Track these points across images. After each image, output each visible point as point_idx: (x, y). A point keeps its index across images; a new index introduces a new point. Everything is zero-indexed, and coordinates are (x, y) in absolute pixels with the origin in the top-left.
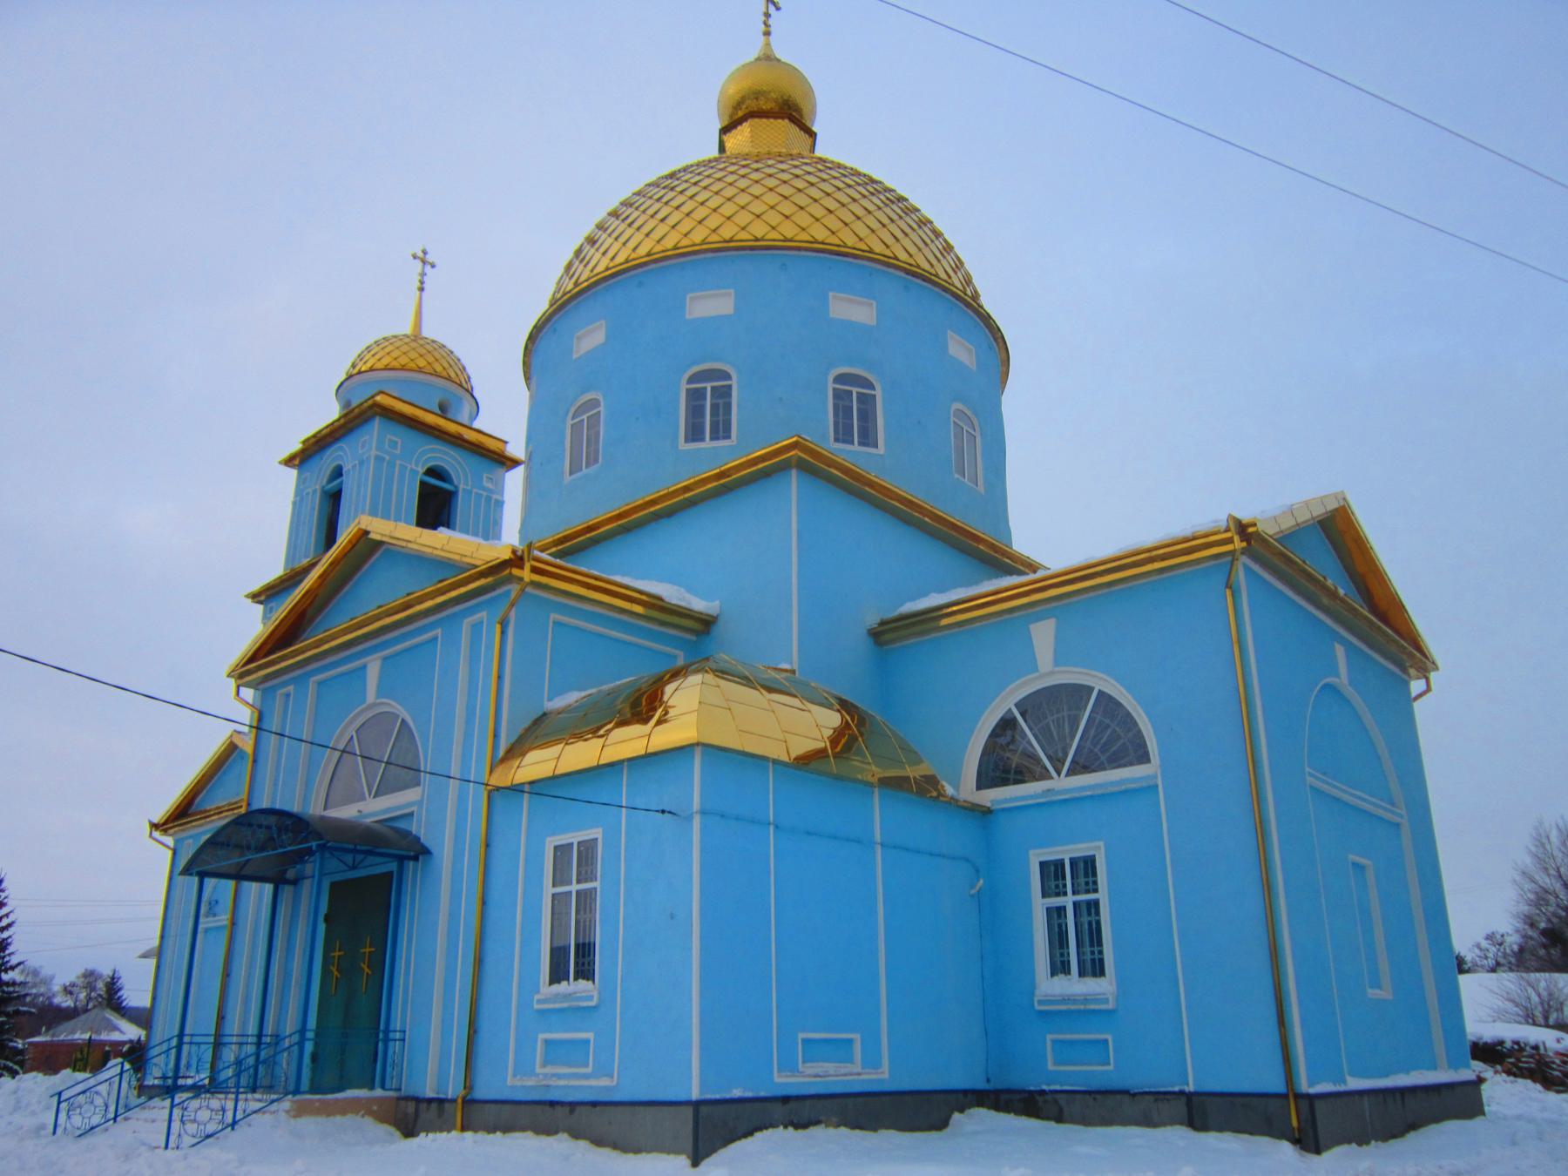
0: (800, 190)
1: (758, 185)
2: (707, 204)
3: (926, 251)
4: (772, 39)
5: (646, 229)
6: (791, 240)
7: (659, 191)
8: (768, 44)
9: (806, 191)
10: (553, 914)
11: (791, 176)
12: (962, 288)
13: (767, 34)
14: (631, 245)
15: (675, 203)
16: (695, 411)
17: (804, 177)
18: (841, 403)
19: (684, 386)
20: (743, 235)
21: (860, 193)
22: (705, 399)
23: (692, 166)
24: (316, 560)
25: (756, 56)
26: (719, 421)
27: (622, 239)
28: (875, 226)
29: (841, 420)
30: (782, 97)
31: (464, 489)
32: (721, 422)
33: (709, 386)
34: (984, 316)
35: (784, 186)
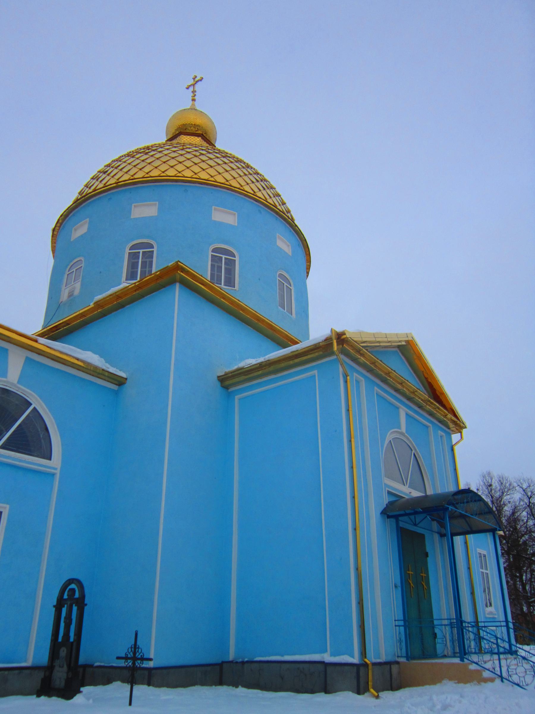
1: (189, 161)
4: (196, 103)
7: (117, 163)
9: (207, 170)
13: (194, 100)
15: (139, 167)
18: (216, 264)
19: (127, 251)
21: (256, 179)
22: (139, 258)
26: (146, 270)
29: (216, 273)
30: (471, 685)
32: (147, 267)
33: (141, 251)
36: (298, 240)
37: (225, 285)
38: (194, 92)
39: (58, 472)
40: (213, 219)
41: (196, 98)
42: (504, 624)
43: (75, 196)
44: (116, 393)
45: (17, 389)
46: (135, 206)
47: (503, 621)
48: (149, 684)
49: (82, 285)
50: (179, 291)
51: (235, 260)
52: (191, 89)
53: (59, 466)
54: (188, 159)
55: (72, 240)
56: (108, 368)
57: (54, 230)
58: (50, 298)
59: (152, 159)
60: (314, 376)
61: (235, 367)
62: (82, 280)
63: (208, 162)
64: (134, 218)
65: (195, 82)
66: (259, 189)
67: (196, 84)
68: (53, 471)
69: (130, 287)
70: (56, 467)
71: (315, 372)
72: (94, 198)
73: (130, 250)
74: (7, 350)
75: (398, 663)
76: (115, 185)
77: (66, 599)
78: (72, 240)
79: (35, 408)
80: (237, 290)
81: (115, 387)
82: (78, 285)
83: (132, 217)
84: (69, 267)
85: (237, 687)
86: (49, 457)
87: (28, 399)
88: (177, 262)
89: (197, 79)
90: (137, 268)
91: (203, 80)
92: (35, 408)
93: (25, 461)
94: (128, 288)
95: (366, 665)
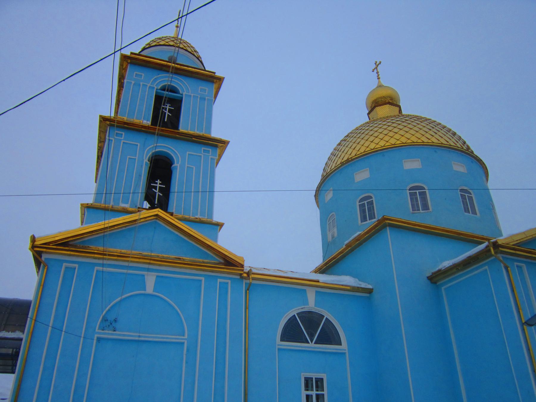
0: (395, 127)
4: (381, 80)
6: (374, 149)
8: (379, 82)
9: (397, 127)
11: (396, 121)
13: (378, 78)
16: (363, 211)
19: (358, 204)
27: (338, 156)
31: (186, 95)
33: (366, 202)
35: (399, 126)
36: (470, 158)
37: (422, 210)
38: (377, 73)
39: (347, 351)
40: (405, 168)
45: (315, 310)
46: (356, 174)
50: (390, 232)
52: (375, 71)
55: (326, 202)
56: (361, 285)
57: (315, 196)
58: (323, 239)
59: (367, 137)
60: (486, 270)
61: (437, 269)
62: (337, 227)
63: (408, 126)
64: (357, 182)
65: (377, 66)
66: (444, 134)
67: (377, 67)
68: (344, 351)
70: (345, 349)
71: (487, 267)
72: (330, 177)
73: (359, 202)
78: (326, 202)
79: (327, 318)
80: (431, 211)
81: (368, 295)
82: (335, 230)
83: (356, 182)
84: (328, 219)
85: (9, 332)
88: (383, 216)
89: (377, 64)
90: (366, 213)
91: (381, 63)
92: (327, 318)
94: (361, 234)
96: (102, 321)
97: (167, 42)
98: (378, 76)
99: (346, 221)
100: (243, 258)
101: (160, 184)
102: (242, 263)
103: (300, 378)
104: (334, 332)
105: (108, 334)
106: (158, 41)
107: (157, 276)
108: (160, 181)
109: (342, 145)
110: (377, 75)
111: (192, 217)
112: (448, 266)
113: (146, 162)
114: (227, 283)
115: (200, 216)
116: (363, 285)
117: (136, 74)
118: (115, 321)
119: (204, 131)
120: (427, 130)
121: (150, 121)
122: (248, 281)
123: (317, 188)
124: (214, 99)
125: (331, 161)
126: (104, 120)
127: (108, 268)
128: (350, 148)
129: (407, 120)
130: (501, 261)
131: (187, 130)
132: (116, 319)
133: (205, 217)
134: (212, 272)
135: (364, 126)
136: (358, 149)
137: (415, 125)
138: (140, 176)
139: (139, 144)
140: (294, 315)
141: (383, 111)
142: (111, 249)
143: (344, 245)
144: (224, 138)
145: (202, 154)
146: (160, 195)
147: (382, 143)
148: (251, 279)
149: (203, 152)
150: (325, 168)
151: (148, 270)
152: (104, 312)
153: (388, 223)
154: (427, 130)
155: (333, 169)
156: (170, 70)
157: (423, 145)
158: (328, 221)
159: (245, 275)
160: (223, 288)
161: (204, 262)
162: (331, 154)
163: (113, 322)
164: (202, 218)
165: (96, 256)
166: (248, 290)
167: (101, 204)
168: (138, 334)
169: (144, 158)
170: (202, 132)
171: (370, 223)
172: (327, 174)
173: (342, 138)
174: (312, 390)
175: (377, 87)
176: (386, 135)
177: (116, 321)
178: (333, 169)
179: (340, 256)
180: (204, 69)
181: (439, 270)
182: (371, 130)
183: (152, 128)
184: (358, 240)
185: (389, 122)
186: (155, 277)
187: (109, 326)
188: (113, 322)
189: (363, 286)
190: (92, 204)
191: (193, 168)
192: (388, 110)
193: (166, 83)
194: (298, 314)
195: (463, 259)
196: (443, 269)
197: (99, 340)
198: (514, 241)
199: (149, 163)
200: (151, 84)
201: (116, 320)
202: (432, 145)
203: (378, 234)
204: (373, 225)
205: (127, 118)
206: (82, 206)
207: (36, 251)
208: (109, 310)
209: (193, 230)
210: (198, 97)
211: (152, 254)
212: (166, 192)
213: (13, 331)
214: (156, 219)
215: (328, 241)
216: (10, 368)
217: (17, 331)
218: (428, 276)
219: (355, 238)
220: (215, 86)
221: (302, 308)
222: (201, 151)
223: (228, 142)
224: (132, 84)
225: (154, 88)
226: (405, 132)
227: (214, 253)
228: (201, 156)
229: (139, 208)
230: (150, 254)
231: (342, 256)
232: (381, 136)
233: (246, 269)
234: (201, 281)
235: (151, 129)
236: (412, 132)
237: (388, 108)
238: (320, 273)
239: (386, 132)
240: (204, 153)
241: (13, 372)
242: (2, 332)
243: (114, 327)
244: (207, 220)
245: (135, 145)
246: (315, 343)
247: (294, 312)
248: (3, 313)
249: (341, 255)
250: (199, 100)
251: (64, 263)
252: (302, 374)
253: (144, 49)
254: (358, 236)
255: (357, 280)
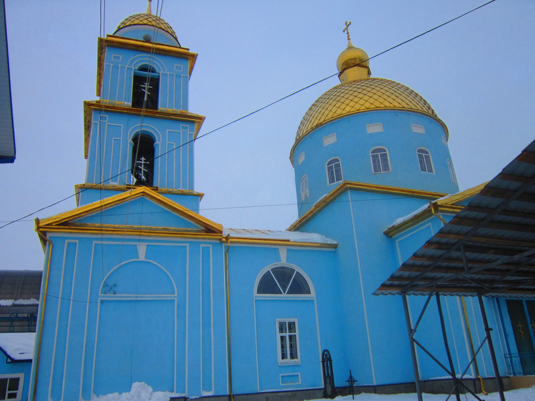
0: (364, 90)
2: (340, 101)
3: (415, 100)
4: (351, 41)
5: (322, 113)
6: (340, 115)
9: (362, 92)
10: (296, 338)
12: (427, 111)
13: (349, 39)
14: (318, 118)
17: (370, 87)
19: (326, 167)
20: (353, 110)
23: (331, 89)
24: (445, 195)
25: (347, 48)
28: (395, 98)
31: (162, 73)
33: (333, 165)
34: (438, 120)
35: (359, 89)
38: (348, 33)
39: (315, 299)
40: (368, 132)
41: (350, 37)
42: (513, 355)
43: (293, 142)
44: (335, 253)
47: (516, 354)
48: (375, 393)
49: (309, 190)
51: (386, 153)
52: (346, 31)
53: (315, 296)
54: (351, 90)
55: (299, 165)
56: (327, 241)
57: (290, 158)
60: (430, 226)
61: (392, 225)
63: (367, 89)
65: (347, 26)
67: (348, 27)
69: (328, 196)
70: (313, 296)
72: (304, 139)
74: (278, 249)
75: (508, 377)
76: (311, 130)
77: (325, 359)
78: (299, 165)
79: (297, 272)
81: (334, 250)
82: (308, 190)
83: (324, 146)
85: (25, 299)
86: (309, 293)
87: (294, 269)
91: (351, 24)
92: (297, 272)
93: (299, 297)
95: (479, 379)
96: (104, 285)
97: (141, 21)
98: (348, 37)
99: (316, 182)
100: (222, 225)
101: (148, 85)
102: (221, 230)
103: (275, 324)
104: (304, 283)
105: (110, 297)
106: (132, 20)
107: (148, 246)
108: (144, 158)
109: (313, 110)
110: (347, 35)
111: (175, 189)
112: (400, 222)
113: (130, 142)
114: (209, 247)
115: (182, 188)
116: (330, 241)
117: (114, 56)
118: (115, 285)
119: (181, 108)
120: (393, 92)
121: (130, 102)
122: (227, 245)
123: (291, 151)
124: (189, 76)
125: (303, 126)
126: (88, 105)
127: (105, 241)
128: (319, 113)
129: (372, 85)
130: (441, 219)
131: (166, 108)
132: (115, 284)
133: (187, 189)
134: (195, 239)
135: (333, 92)
136: (335, 104)
137: (379, 90)
138: (126, 155)
139: (122, 126)
140: (269, 271)
141: (354, 73)
142: (106, 225)
143: (313, 206)
144: (200, 114)
145: (180, 130)
146: (146, 172)
147: (348, 109)
148: (229, 243)
149: (182, 129)
150: (300, 126)
151: (139, 241)
152: (105, 278)
153: (350, 187)
154: (393, 92)
155: (305, 133)
156: (144, 109)
157: (386, 109)
158: (301, 182)
159: (224, 240)
160: (206, 251)
161: (187, 231)
162: (306, 113)
163: (113, 286)
164: (184, 190)
165: (93, 232)
166: (227, 252)
167: (93, 183)
168: (135, 295)
169: (128, 138)
170: (180, 109)
171: (337, 184)
172: (299, 138)
173: (313, 102)
174: (286, 332)
175: (347, 49)
176: (352, 100)
177: (115, 285)
178: (304, 134)
179: (310, 215)
180: (179, 46)
181: (393, 226)
182: (338, 96)
183: (133, 109)
184: (324, 202)
185: (358, 85)
186: (146, 246)
187: (110, 290)
188: (113, 286)
189: (329, 242)
190: (84, 185)
191: (173, 144)
192: (357, 72)
193: (139, 130)
194: (272, 270)
195: (411, 217)
196: (396, 225)
197: (102, 302)
198: (453, 201)
199: (132, 142)
200: (129, 66)
201: (115, 284)
202: (394, 110)
203: (341, 196)
204: (336, 189)
205: (109, 100)
206: (77, 187)
207: (41, 232)
208: (109, 277)
209: (176, 204)
210: (174, 75)
211: (142, 227)
212: (150, 167)
213: (29, 298)
214: (143, 195)
215: (302, 200)
216: (27, 328)
217: (32, 298)
218: (384, 231)
219: (322, 200)
220: (189, 64)
221: (275, 265)
222: (181, 129)
223: (204, 118)
224: (111, 67)
225: (131, 69)
226: (369, 97)
227: (196, 222)
228: (180, 133)
229: (127, 185)
230: (140, 227)
231: (306, 219)
232: (347, 102)
233: (225, 234)
234: (186, 246)
235: (131, 111)
236: (376, 97)
237: (357, 70)
238: (294, 231)
239: (351, 97)
240: (182, 130)
241: (35, 332)
242: (19, 300)
243: (114, 291)
244: (189, 192)
245: (119, 126)
246: (287, 294)
247: (268, 268)
248: (18, 284)
249: (311, 214)
250: (175, 77)
251: (66, 239)
252: (277, 319)
253: (119, 29)
254: (324, 198)
255: (324, 237)
